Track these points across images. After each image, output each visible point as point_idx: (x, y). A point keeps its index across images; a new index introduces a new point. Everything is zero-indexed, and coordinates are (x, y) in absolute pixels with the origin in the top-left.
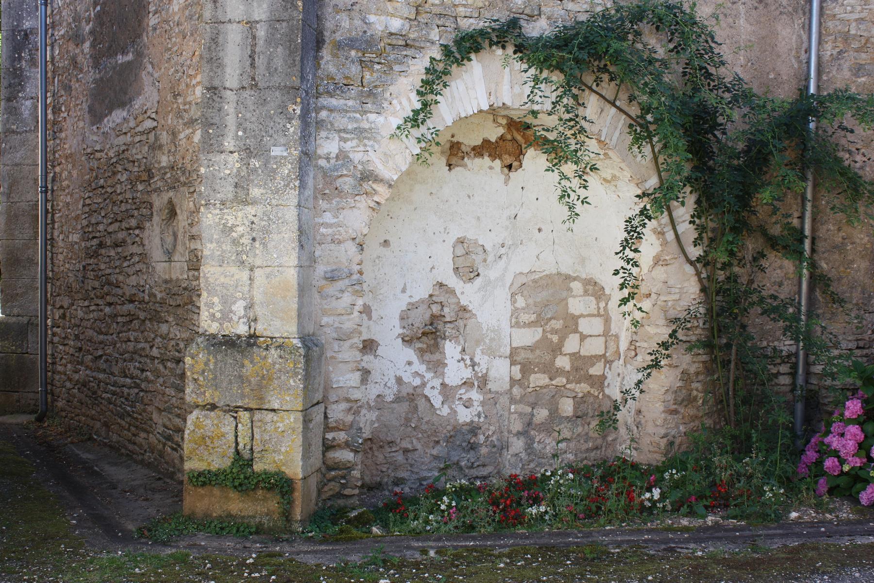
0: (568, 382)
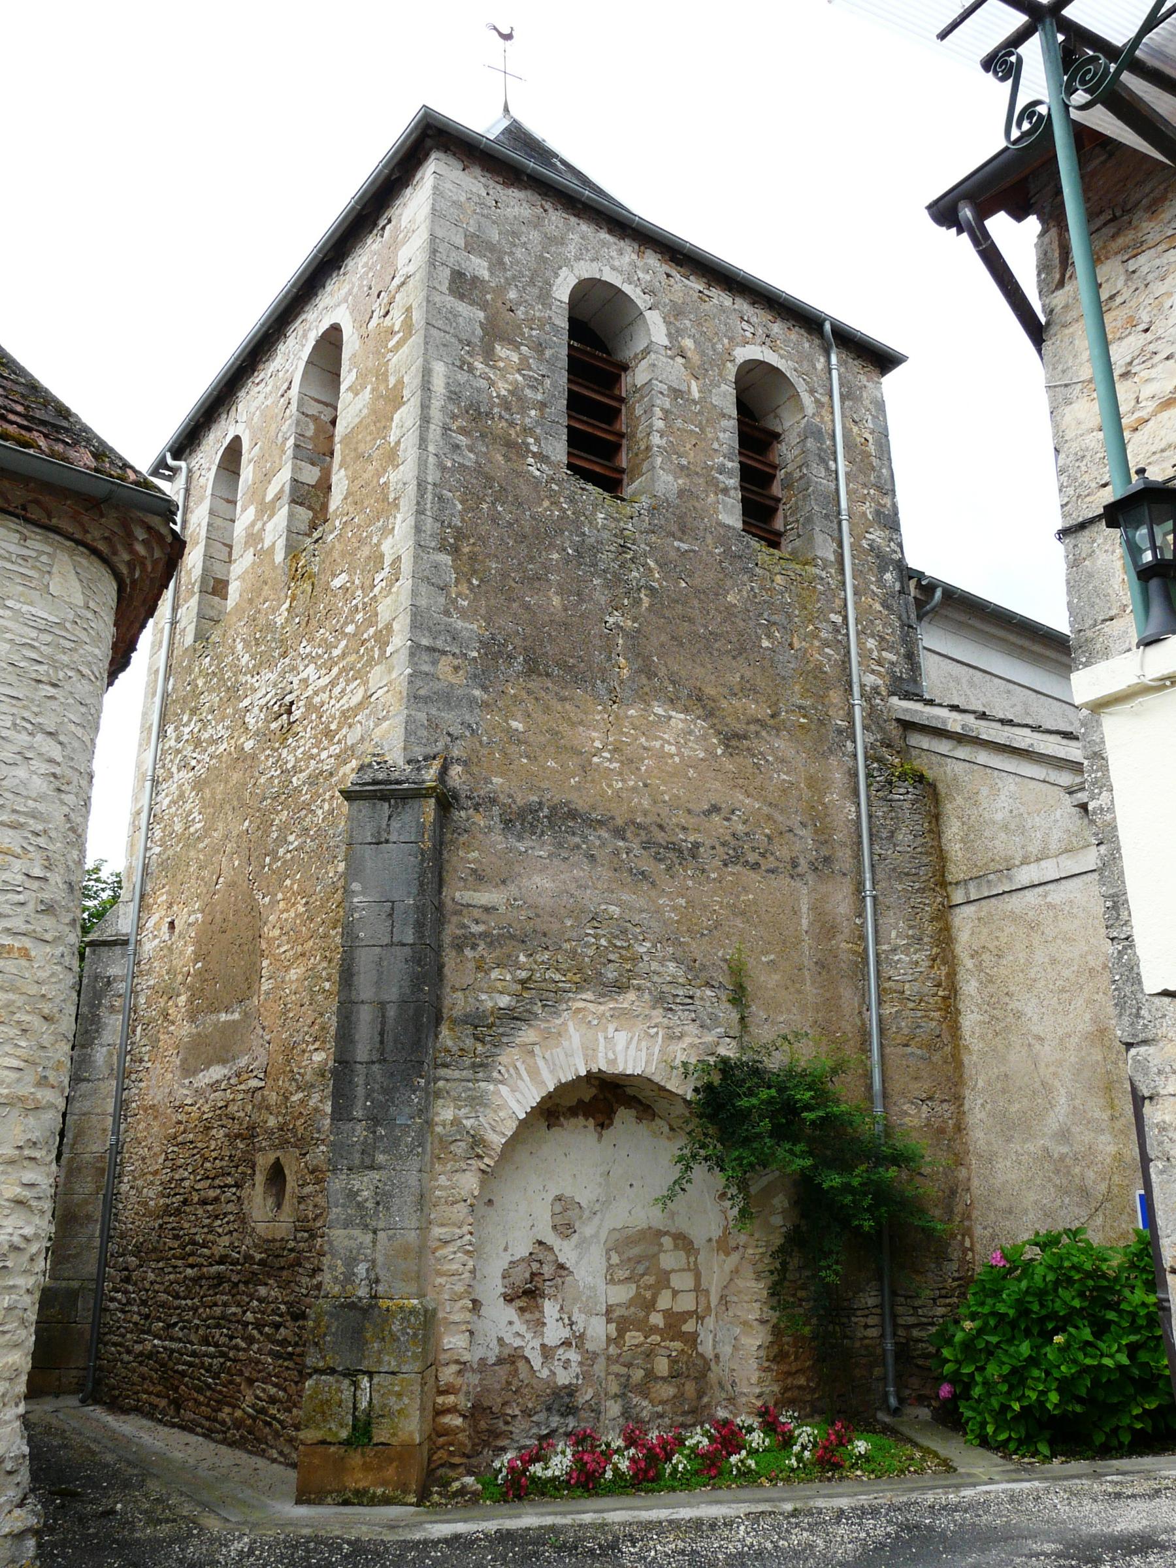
0: (663, 1340)
